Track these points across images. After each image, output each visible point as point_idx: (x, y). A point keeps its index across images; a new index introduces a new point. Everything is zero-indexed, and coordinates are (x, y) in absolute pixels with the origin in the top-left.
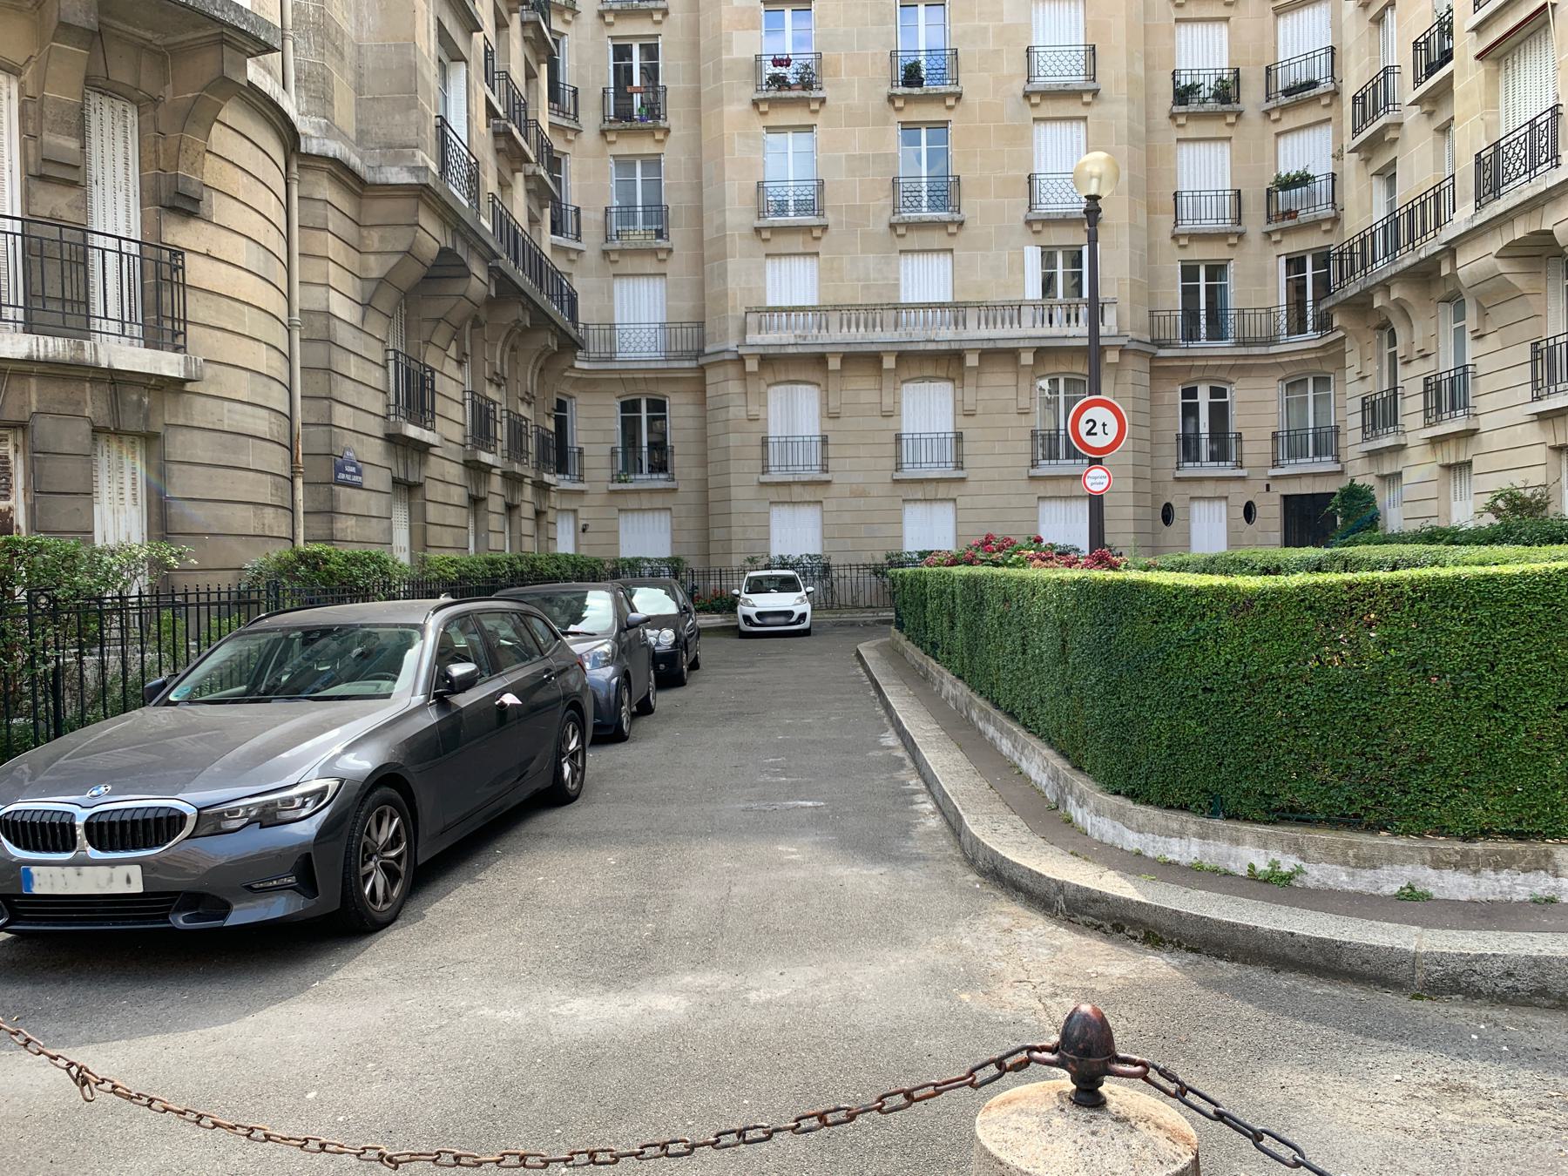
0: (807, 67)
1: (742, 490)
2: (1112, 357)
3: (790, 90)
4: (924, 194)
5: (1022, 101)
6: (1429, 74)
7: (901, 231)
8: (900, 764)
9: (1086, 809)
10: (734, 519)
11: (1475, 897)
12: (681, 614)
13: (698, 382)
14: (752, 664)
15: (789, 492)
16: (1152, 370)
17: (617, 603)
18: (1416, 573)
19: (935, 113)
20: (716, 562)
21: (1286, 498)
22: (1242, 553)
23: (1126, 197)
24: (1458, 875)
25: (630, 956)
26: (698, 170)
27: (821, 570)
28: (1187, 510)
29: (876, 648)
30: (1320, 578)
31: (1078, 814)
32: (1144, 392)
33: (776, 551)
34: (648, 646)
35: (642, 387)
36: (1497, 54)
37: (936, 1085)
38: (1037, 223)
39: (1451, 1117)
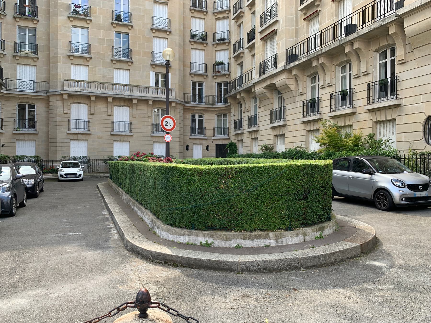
0: (86, 9)
1: (61, 135)
2: (174, 105)
3: (80, 15)
4: (121, 52)
5: (150, 31)
6: (250, 42)
7: (17, 58)
8: (107, 219)
9: (159, 230)
10: (58, 144)
11: (253, 246)
12: (37, 174)
13: (47, 100)
14: (62, 190)
15: (77, 136)
16: (184, 109)
17: (12, 170)
18: (240, 165)
19: (125, 30)
20: (51, 158)
21: (216, 145)
22: (204, 159)
23: (178, 61)
24: (249, 241)
25: (9, 287)
26: (48, 34)
27: (86, 161)
28: (192, 147)
29: (103, 185)
30: (222, 166)
31: (158, 231)
32: (182, 115)
33: (72, 155)
34: (24, 185)
35: (26, 101)
36: (265, 39)
37: (99, 318)
38: (154, 65)
39: (244, 303)
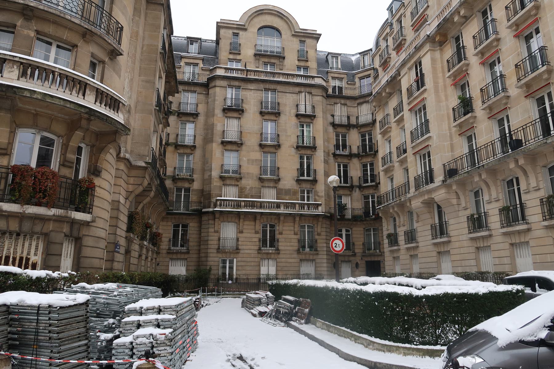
21: (366, 262)
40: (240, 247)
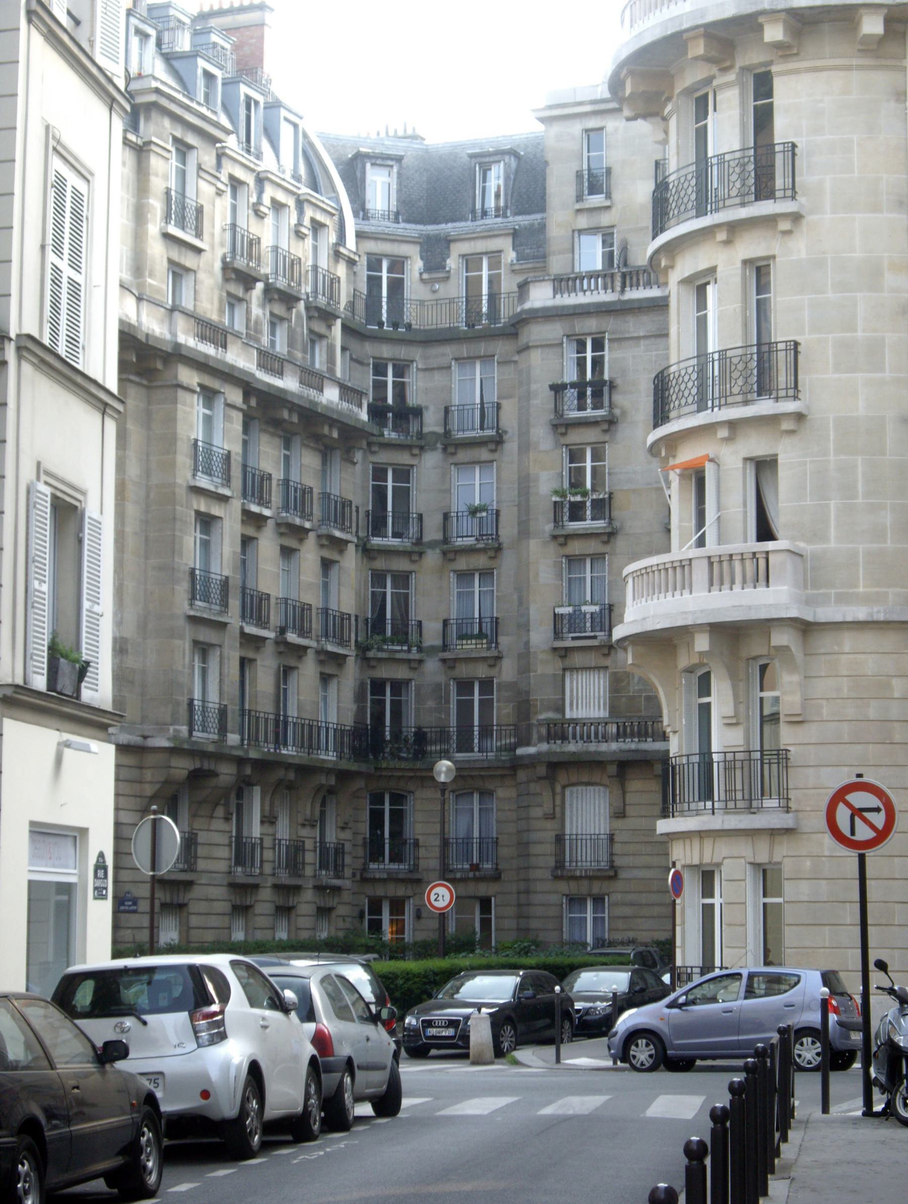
40: (618, 862)
